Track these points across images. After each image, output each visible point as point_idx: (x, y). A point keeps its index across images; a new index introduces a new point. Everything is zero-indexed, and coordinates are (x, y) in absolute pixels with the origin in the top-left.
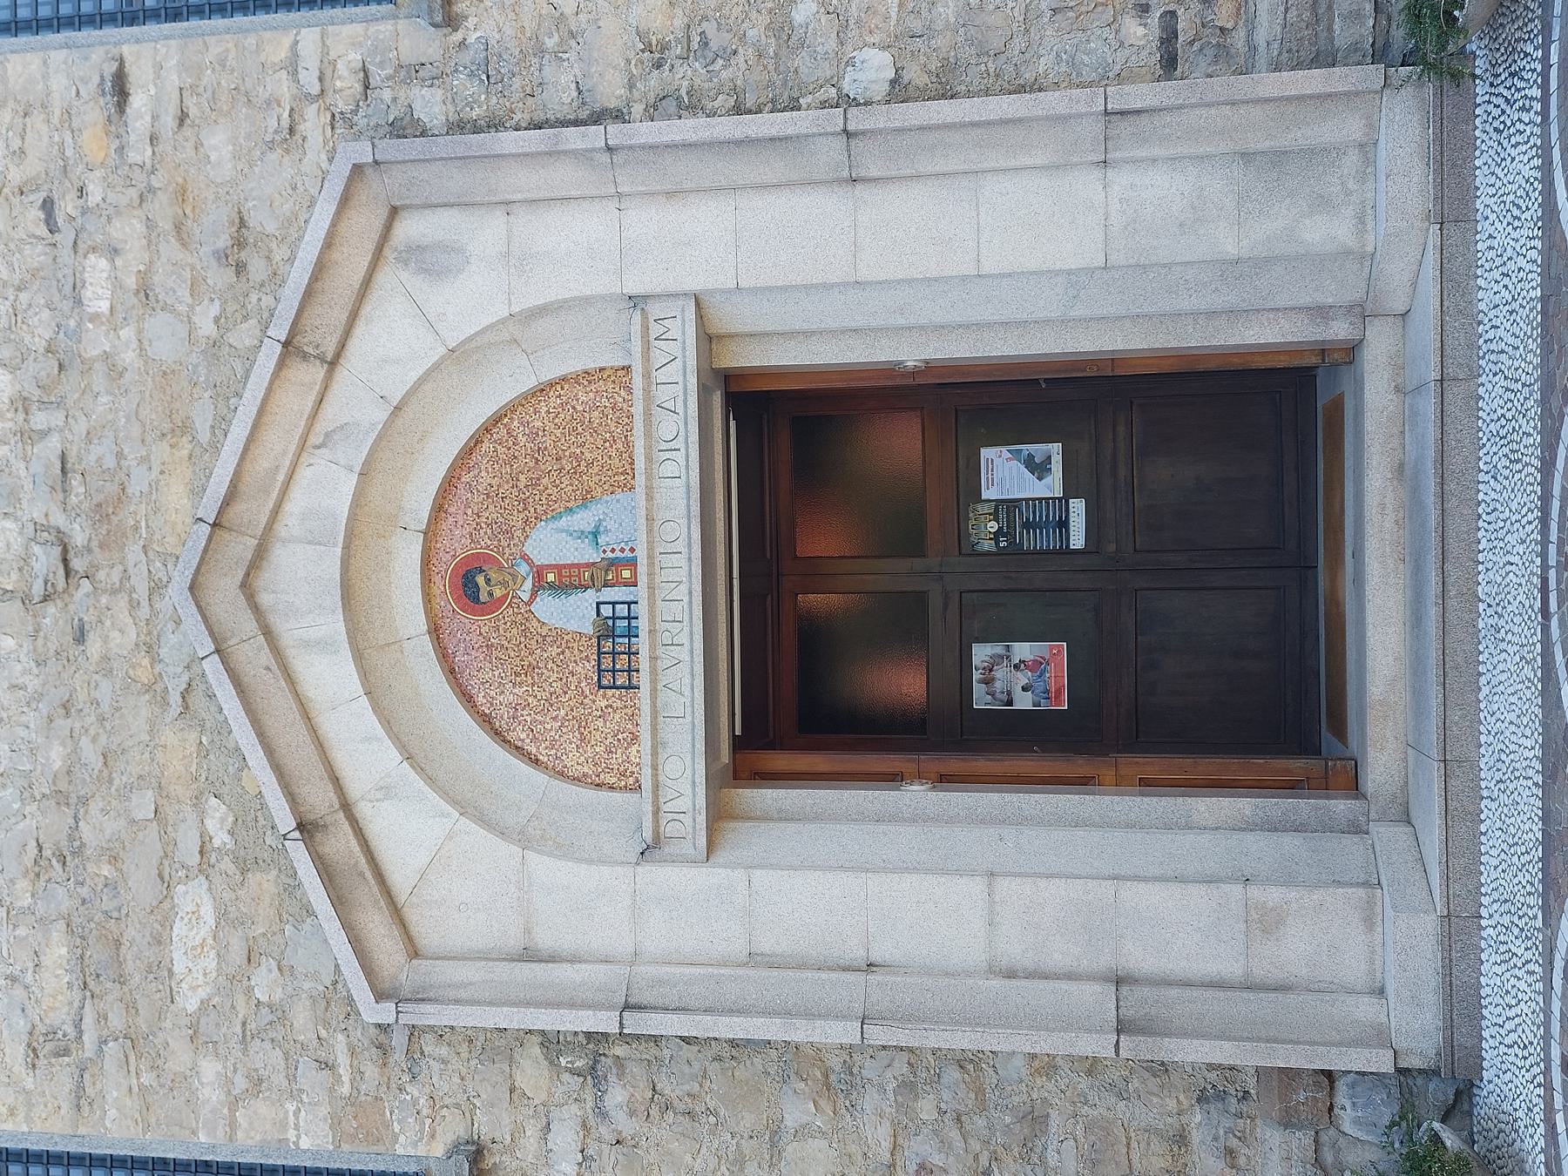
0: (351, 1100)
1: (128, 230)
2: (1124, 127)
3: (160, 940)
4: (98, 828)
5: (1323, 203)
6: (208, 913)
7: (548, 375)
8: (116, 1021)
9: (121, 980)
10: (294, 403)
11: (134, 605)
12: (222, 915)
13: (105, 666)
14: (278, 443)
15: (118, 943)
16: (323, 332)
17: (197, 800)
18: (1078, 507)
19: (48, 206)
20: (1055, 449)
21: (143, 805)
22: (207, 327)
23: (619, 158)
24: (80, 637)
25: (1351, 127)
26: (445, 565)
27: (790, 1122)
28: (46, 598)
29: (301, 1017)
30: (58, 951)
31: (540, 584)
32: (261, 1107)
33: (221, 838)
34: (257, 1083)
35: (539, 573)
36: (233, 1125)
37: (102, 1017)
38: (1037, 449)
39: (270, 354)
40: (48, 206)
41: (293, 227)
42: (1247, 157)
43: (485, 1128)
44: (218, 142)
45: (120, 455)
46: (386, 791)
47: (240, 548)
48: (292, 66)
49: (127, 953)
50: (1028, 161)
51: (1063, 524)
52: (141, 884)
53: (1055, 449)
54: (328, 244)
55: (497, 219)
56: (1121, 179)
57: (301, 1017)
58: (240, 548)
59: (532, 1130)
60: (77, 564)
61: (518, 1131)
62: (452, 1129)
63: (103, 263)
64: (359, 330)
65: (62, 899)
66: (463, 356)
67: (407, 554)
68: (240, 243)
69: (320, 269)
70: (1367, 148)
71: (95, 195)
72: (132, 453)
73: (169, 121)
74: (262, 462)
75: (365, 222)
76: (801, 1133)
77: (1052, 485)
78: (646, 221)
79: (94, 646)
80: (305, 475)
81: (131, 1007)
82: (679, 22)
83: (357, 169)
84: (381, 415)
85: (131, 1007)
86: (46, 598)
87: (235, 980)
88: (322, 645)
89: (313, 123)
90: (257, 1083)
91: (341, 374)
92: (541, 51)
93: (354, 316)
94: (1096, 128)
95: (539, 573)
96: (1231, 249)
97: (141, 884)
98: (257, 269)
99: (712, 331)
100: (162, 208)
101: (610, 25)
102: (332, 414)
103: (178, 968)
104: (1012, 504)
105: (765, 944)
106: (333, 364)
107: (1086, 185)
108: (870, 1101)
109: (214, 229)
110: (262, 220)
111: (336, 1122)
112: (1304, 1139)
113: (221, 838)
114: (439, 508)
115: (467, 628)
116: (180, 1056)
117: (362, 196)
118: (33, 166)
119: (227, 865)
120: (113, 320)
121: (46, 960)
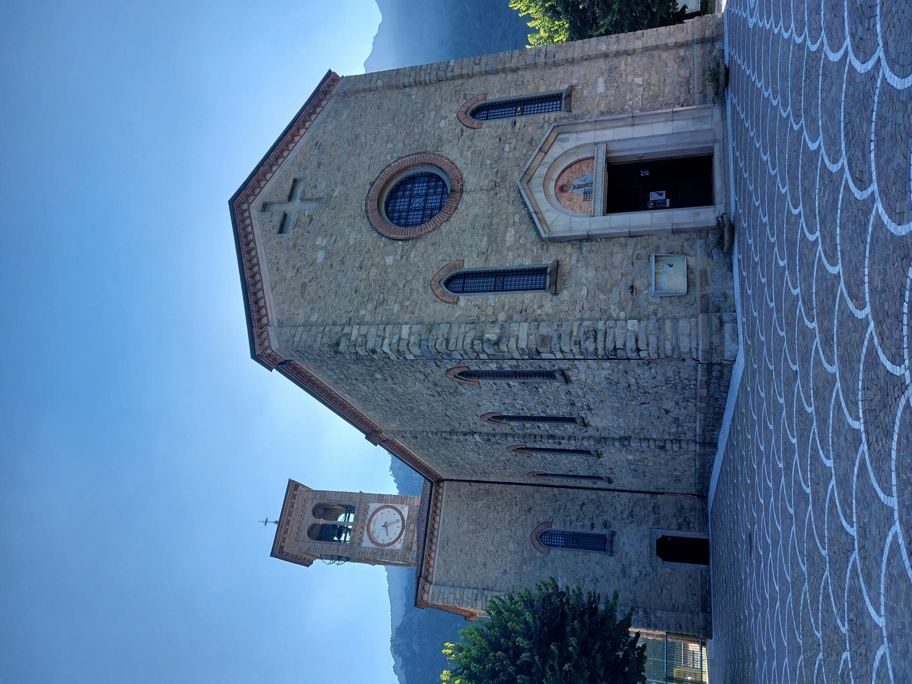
0: (536, 256)
1: (514, 141)
2: (675, 114)
3: (504, 236)
4: (495, 221)
5: (706, 123)
6: (513, 232)
7: (580, 157)
8: (494, 249)
9: (496, 242)
10: (539, 158)
11: (506, 190)
12: (516, 232)
13: (500, 199)
14: (536, 163)
15: (496, 237)
16: (546, 148)
17: (514, 215)
18: (668, 201)
19: (500, 139)
20: (664, 192)
21: (504, 217)
22: (524, 151)
23: (597, 123)
24: (496, 194)
25: (709, 113)
26: (558, 187)
27: (615, 251)
28: (491, 190)
29: (528, 245)
30: (485, 239)
31: (574, 187)
32: (519, 259)
33: (517, 220)
34: (519, 256)
35: (574, 186)
36: (513, 262)
37: (492, 248)
38: (661, 192)
39: (537, 150)
40: (500, 139)
41: (540, 139)
42: (694, 118)
43: (559, 258)
44: (530, 129)
45: (507, 169)
46: (548, 210)
47: (528, 177)
48: (544, 118)
49: (498, 239)
50: (660, 120)
51: (665, 203)
52: (502, 228)
53: (664, 192)
54: (548, 136)
55: (575, 134)
56: (675, 123)
57: (528, 245)
58: (528, 177)
59: (568, 258)
60: (497, 185)
61: (566, 258)
62: (553, 259)
63: (508, 145)
64: (551, 149)
65: (488, 231)
66: (566, 153)
67: (553, 184)
68: (531, 141)
69: (547, 139)
70: (712, 116)
71: (508, 136)
72: (509, 169)
73: (523, 126)
74: (533, 166)
75: (554, 134)
76: (617, 253)
77: (664, 197)
78: (599, 133)
79: (498, 196)
80: (539, 169)
81: (498, 246)
82: (606, 109)
83: (555, 127)
84: (553, 160)
85: (498, 246)
86: (491, 190)
87: (517, 240)
88: (539, 192)
89: (546, 125)
90: (519, 256)
91: (546, 156)
92: (584, 114)
93: (549, 148)
94: (670, 115)
95: (574, 186)
96: (692, 129)
97: (502, 228)
98: (534, 144)
99: (609, 149)
100: (519, 138)
101: (595, 110)
102: (544, 161)
103: (507, 240)
104: (656, 201)
105: (612, 226)
106: (546, 154)
107: (670, 123)
108: (629, 247)
109: (528, 138)
110: (535, 138)
111: (532, 260)
112: (703, 241)
113: (517, 220)
114: (558, 178)
115: (560, 194)
116: (505, 253)
117: (554, 131)
118: (499, 133)
119: (518, 224)
120: (509, 152)
121: (483, 241)
